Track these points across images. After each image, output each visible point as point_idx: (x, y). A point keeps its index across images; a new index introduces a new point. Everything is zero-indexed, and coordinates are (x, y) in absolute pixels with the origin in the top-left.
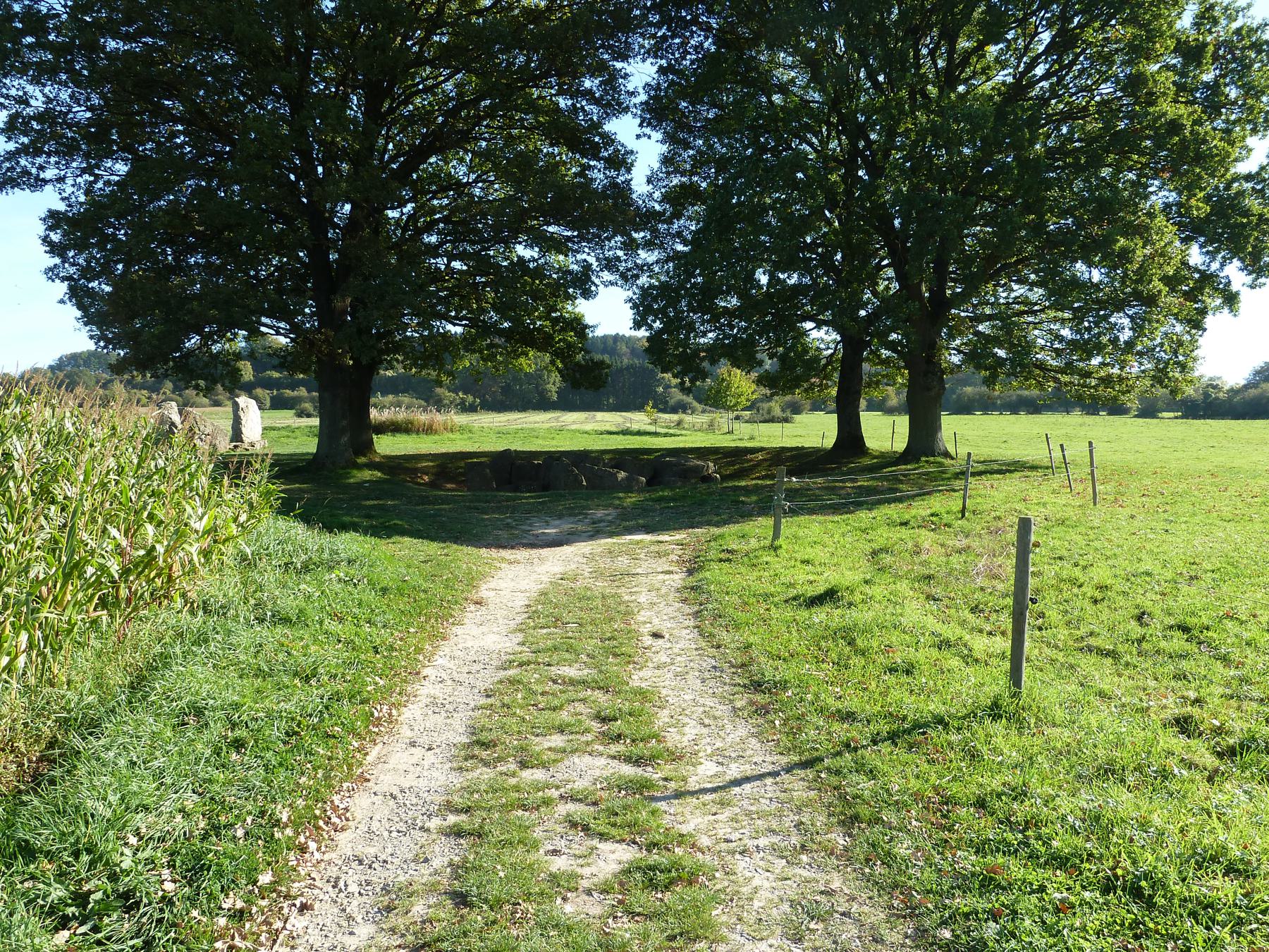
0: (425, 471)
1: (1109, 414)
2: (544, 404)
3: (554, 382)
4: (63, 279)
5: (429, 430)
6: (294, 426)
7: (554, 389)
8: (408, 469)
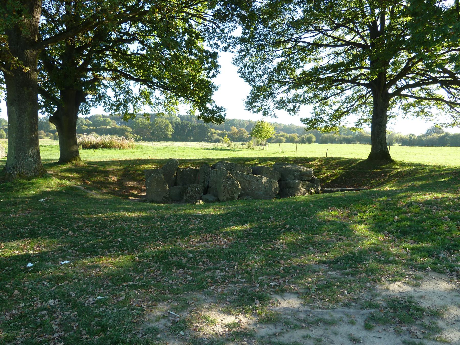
0: (114, 173)
2: (166, 139)
4: (391, 291)
5: (121, 147)
6: (53, 145)
7: (170, 133)
8: (101, 172)
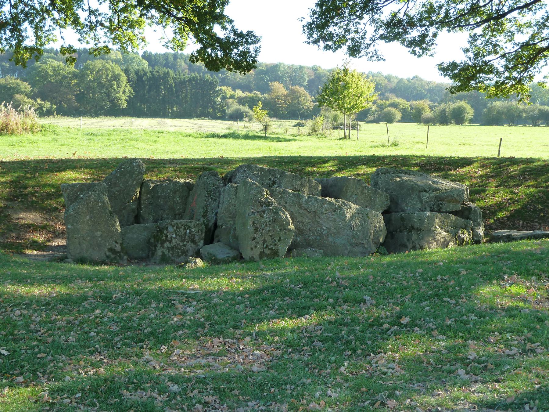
1: (533, 126)
2: (115, 111)
3: (470, 113)
7: (124, 97)
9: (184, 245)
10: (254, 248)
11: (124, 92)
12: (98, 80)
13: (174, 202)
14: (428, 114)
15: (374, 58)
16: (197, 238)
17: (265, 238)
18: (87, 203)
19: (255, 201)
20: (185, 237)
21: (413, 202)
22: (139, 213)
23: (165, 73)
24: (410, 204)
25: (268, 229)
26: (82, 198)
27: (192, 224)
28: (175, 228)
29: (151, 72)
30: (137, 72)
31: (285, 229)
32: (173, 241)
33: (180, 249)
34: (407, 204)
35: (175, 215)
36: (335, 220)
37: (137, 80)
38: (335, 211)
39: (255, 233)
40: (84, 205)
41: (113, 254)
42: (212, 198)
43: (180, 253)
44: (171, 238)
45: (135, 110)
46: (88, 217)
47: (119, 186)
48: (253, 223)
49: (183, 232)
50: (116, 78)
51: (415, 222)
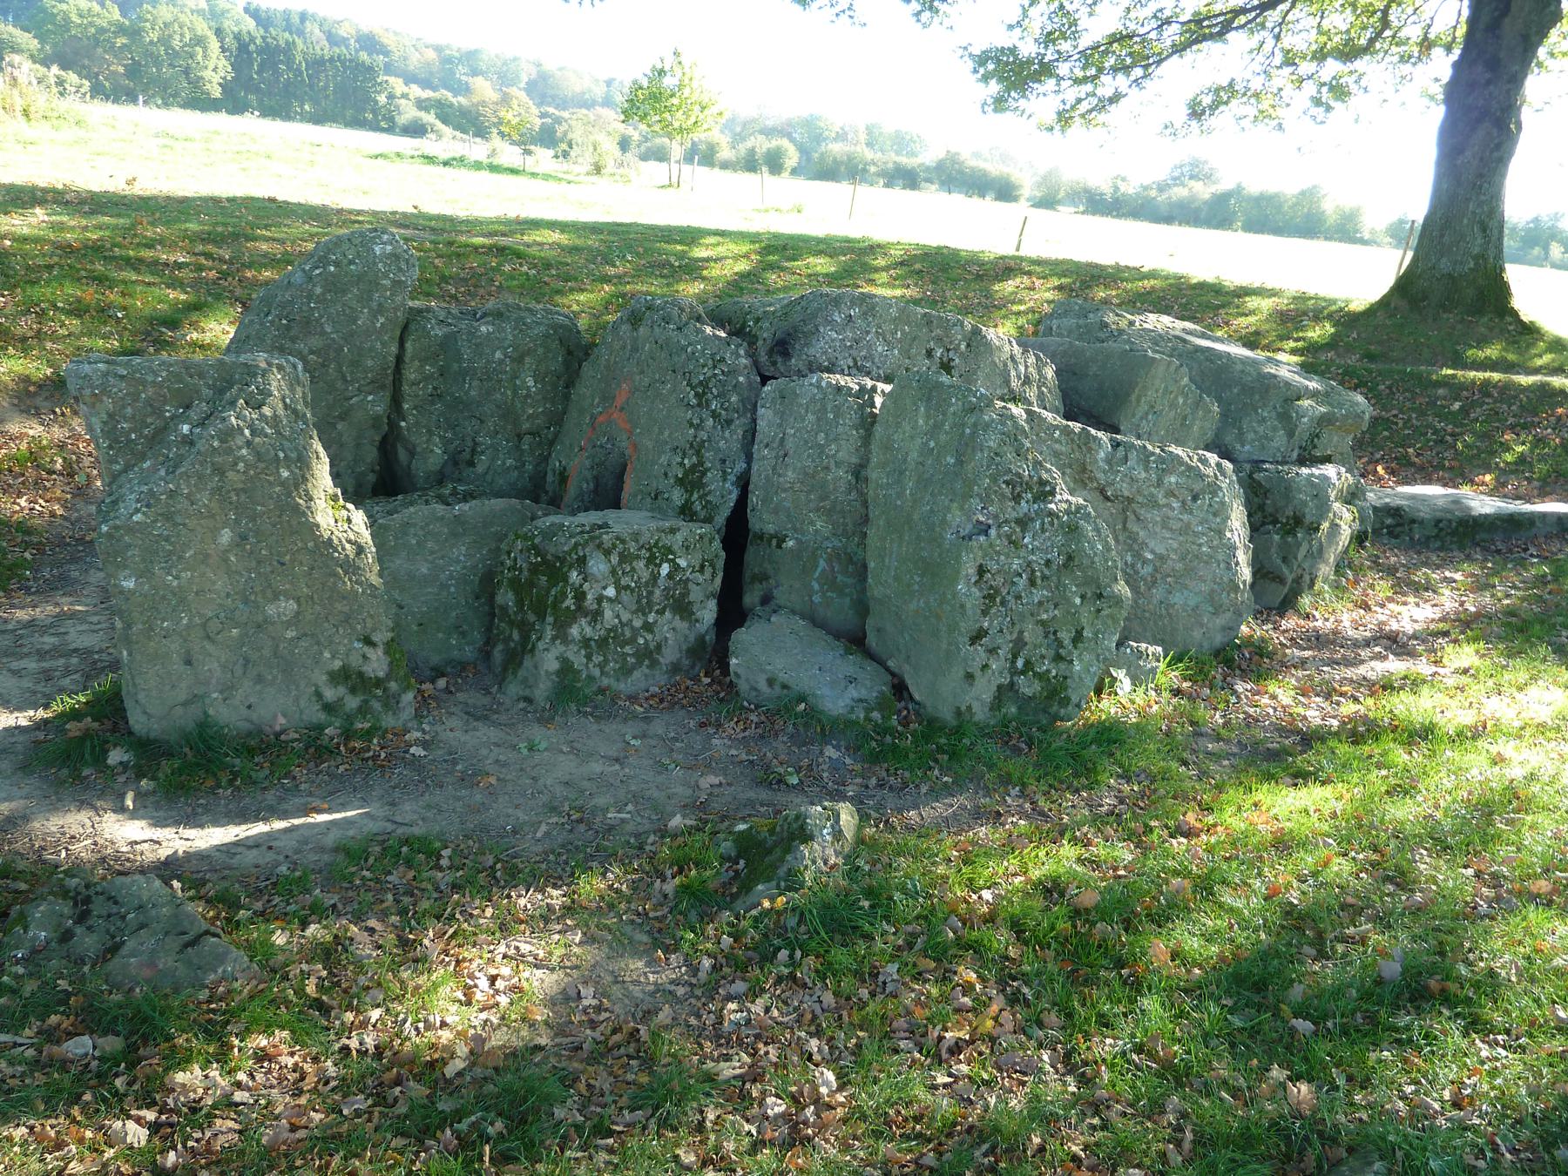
2: (200, 102)
7: (216, 79)
9: (648, 627)
10: (978, 673)
11: (215, 71)
12: (165, 41)
13: (515, 392)
14: (725, 153)
15: (844, 17)
16: (695, 594)
17: (1021, 632)
18: (220, 471)
19: (994, 479)
20: (650, 593)
21: (1261, 429)
22: (393, 425)
23: (287, 42)
24: (1251, 436)
25: (1039, 594)
26: (189, 441)
27: (679, 537)
28: (615, 559)
29: (264, 38)
30: (237, 37)
31: (1100, 596)
32: (608, 614)
33: (632, 641)
34: (1241, 433)
35: (520, 437)
36: (1186, 529)
37: (239, 49)
38: (1195, 498)
39: (985, 613)
40: (200, 477)
41: (353, 691)
42: (714, 415)
43: (631, 660)
44: (600, 599)
45: (233, 101)
46: (226, 536)
47: (323, 333)
48: (981, 571)
49: (645, 575)
50: (199, 41)
51: (1305, 503)
